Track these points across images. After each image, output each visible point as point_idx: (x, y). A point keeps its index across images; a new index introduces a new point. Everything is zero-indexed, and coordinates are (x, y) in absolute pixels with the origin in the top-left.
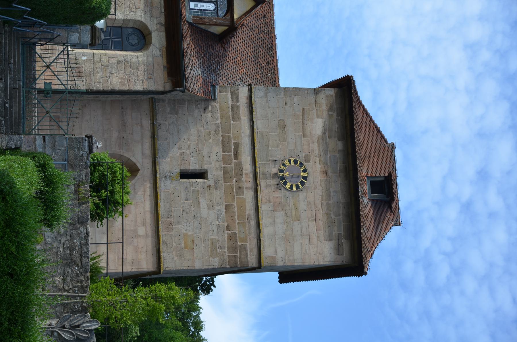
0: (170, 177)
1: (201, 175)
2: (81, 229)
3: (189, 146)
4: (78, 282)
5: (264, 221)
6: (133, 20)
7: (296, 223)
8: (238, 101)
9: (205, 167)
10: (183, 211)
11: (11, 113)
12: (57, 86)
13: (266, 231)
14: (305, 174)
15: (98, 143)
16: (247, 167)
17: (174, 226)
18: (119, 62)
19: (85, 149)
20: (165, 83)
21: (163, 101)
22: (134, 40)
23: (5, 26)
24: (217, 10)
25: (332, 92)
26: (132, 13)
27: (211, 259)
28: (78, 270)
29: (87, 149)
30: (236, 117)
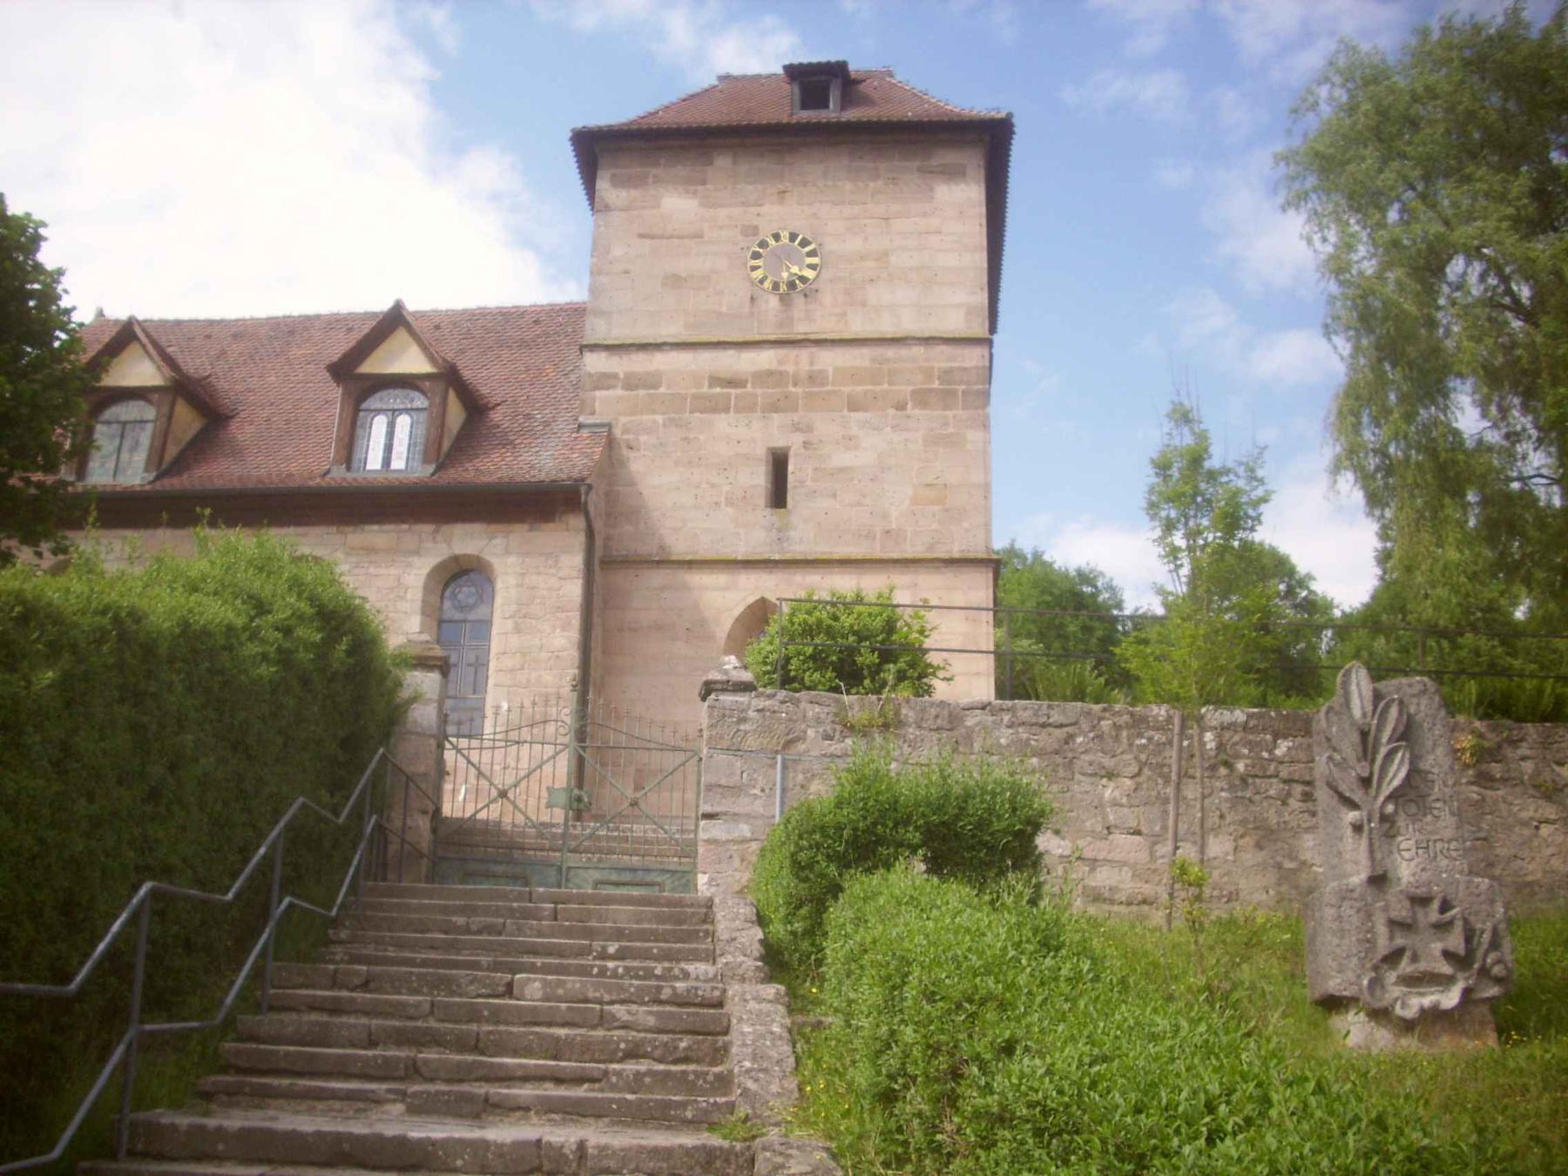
0: (780, 530)
1: (779, 464)
2: (970, 722)
3: (713, 486)
4: (1117, 738)
5: (886, 327)
6: (425, 595)
7: (893, 259)
8: (615, 376)
9: (761, 452)
10: (859, 504)
11: (643, 935)
12: (560, 770)
13: (910, 324)
14: (785, 236)
15: (727, 667)
16: (765, 359)
17: (894, 526)
18: (518, 630)
19: (742, 703)
20: (567, 530)
21: (608, 538)
22: (465, 592)
23: (334, 938)
24: (412, 409)
25: (603, 184)
26: (409, 596)
27: (969, 446)
28: (1085, 736)
29: (742, 698)
30: (650, 381)
